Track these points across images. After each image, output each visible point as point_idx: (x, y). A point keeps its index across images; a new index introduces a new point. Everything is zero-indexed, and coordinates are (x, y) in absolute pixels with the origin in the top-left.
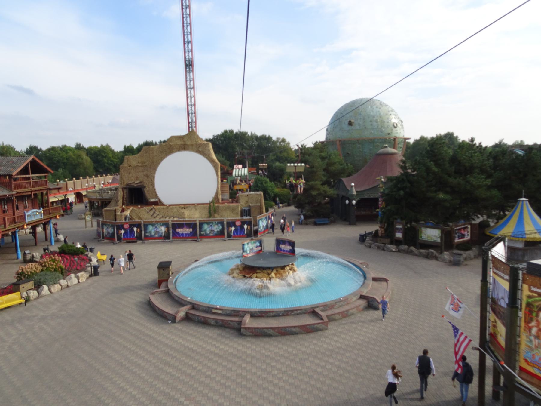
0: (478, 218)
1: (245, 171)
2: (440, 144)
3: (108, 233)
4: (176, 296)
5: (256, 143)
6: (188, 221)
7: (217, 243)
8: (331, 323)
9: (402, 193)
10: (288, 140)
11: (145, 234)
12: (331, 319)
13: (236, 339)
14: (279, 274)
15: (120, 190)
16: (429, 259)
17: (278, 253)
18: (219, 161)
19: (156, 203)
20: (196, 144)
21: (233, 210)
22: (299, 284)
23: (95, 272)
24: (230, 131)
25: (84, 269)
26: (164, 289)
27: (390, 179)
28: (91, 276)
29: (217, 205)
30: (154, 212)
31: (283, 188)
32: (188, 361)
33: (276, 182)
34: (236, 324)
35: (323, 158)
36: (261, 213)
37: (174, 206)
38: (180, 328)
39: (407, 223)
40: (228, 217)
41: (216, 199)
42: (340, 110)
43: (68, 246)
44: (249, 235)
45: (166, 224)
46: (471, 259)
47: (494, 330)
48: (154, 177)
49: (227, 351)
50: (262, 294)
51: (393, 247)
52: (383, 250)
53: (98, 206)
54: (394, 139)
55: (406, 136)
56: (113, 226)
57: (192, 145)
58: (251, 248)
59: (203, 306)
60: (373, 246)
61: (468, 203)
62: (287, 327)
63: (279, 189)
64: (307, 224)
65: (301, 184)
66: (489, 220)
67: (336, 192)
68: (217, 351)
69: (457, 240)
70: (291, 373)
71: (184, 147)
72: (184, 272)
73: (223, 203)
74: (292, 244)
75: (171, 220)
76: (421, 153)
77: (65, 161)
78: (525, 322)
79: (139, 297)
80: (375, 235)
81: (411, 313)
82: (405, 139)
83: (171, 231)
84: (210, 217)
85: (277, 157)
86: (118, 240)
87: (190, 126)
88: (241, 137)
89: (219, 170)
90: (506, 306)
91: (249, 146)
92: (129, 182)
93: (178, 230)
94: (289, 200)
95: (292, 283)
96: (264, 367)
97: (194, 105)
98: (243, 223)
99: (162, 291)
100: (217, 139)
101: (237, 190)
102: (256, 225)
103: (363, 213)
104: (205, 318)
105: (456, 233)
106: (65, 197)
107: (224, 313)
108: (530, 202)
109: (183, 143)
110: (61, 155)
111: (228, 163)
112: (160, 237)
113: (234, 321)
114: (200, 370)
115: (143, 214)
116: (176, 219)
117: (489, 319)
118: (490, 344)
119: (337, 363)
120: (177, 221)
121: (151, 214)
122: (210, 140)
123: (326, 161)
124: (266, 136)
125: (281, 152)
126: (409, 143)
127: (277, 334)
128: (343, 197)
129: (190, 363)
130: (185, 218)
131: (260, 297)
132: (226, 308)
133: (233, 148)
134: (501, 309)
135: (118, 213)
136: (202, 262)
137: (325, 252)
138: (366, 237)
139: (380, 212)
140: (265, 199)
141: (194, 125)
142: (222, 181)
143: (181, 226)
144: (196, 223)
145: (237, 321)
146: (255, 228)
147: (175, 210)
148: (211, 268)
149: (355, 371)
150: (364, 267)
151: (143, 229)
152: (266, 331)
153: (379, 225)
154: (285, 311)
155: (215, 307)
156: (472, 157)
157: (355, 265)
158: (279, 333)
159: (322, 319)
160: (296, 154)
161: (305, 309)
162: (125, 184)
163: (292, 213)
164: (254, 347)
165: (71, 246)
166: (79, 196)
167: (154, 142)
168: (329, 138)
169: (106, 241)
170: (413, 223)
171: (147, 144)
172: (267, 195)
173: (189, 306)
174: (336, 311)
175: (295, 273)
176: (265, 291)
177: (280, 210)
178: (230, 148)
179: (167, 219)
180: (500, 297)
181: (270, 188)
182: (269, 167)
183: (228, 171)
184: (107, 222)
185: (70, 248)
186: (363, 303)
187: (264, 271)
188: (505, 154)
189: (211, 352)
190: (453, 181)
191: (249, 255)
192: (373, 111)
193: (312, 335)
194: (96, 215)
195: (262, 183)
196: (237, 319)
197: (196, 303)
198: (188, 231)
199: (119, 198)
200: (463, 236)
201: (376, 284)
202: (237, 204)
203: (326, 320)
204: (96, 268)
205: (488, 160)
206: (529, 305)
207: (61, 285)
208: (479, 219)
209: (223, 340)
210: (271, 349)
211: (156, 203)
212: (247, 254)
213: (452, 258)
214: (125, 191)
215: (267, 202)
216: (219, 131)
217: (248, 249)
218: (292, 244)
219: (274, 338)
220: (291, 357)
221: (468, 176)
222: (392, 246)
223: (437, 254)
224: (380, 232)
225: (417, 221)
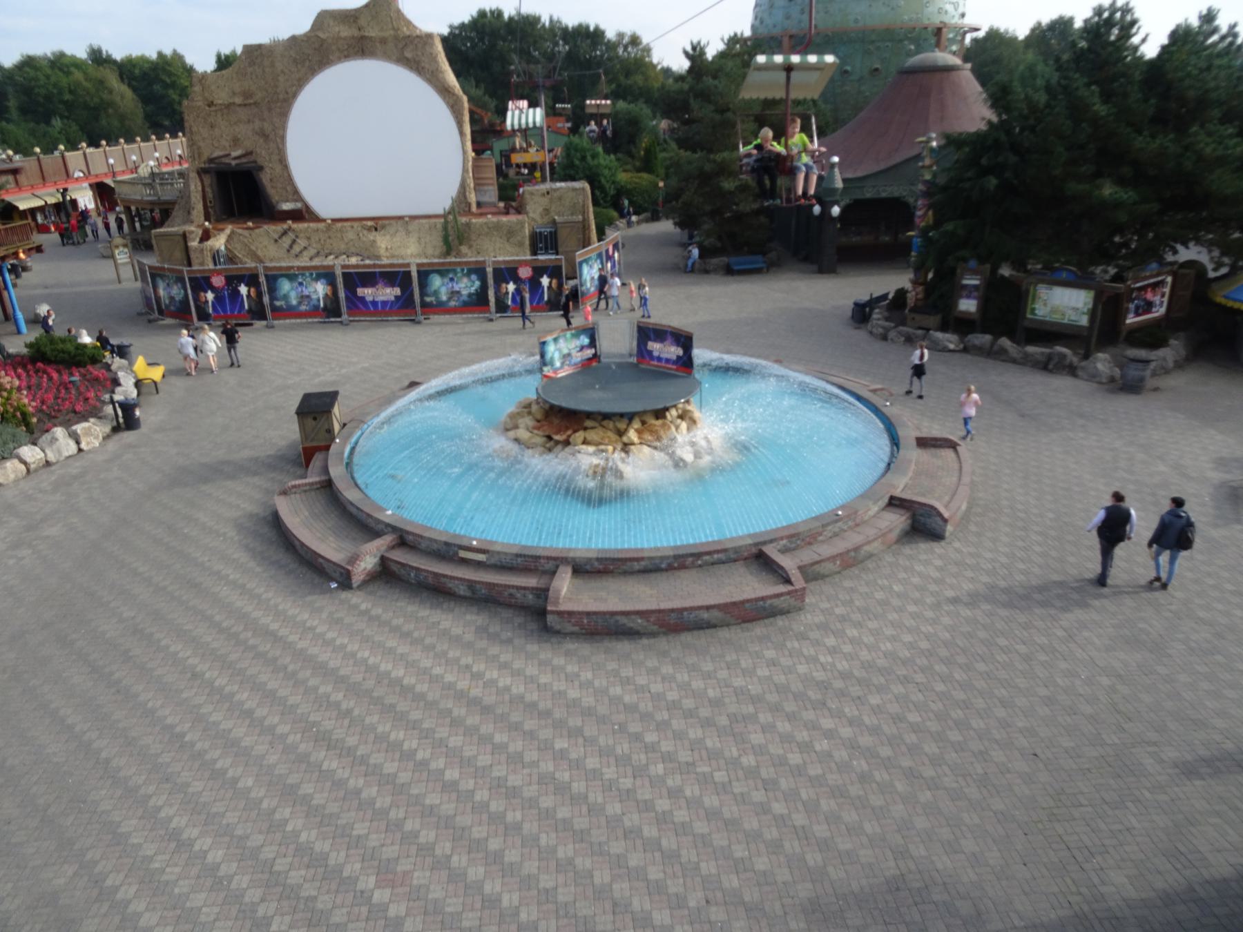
1: (536, 116)
3: (172, 298)
4: (351, 504)
5: (563, 48)
6: (384, 266)
7: (470, 327)
9: (993, 182)
10: (645, 40)
11: (272, 304)
12: (811, 573)
13: (532, 647)
14: (652, 432)
15: (193, 175)
16: (1051, 371)
17: (643, 366)
18: (465, 92)
20: (396, 38)
21: (510, 233)
22: (706, 460)
23: (127, 419)
24: (492, 12)
25: (94, 412)
26: (317, 479)
27: (953, 142)
28: (116, 429)
29: (464, 220)
30: (294, 242)
31: (639, 170)
32: (388, 727)
33: (620, 155)
34: (531, 597)
36: (586, 243)
37: (345, 224)
38: (363, 607)
40: (497, 253)
43: (52, 341)
45: (327, 276)
46: (1167, 372)
48: (283, 138)
49: (507, 689)
50: (603, 495)
51: (950, 340)
53: (142, 219)
56: (180, 280)
57: (383, 41)
58: (565, 351)
59: (431, 540)
60: (892, 334)
62: (685, 609)
63: (630, 175)
64: (706, 272)
68: (476, 692)
69: (1131, 320)
70: (706, 769)
71: (360, 48)
72: (377, 420)
73: (481, 215)
74: (685, 341)
75: (338, 263)
76: (1058, 60)
77: (67, 97)
79: (243, 498)
81: (1037, 549)
83: (342, 294)
84: (448, 253)
85: (619, 86)
86: (200, 319)
88: (524, 29)
89: (467, 118)
91: (544, 54)
92: (216, 154)
93: (361, 291)
94: (655, 203)
95: (689, 457)
96: (623, 748)
98: (539, 271)
99: (311, 484)
102: (572, 276)
103: (855, 239)
104: (436, 575)
105: (1132, 300)
106: (64, 195)
107: (493, 561)
109: (356, 33)
110: (53, 79)
111: (492, 104)
112: (315, 312)
113: (525, 588)
114: (424, 764)
115: (263, 245)
116: (354, 260)
119: (846, 732)
120: (357, 266)
121: (286, 245)
124: (588, 27)
125: (628, 74)
127: (655, 628)
129: (393, 736)
130: (378, 257)
131: (601, 501)
132: (497, 548)
133: (505, 62)
135: (194, 244)
138: (872, 310)
140: (596, 203)
143: (369, 279)
144: (409, 273)
145: (533, 589)
147: (351, 235)
149: (906, 762)
151: (265, 288)
152: (623, 620)
153: (911, 276)
154: (676, 557)
155: (465, 543)
156: (1209, 68)
158: (661, 626)
159: (788, 581)
161: (736, 550)
162: (205, 157)
163: (663, 241)
164: (589, 675)
165: (63, 341)
166: (103, 192)
168: (760, 31)
169: (169, 321)
172: (597, 193)
173: (388, 539)
174: (826, 550)
179: (330, 261)
183: (492, 125)
184: (163, 269)
185: (61, 346)
186: (897, 521)
187: (605, 423)
189: (460, 695)
190: (1146, 144)
191: (561, 374)
193: (758, 629)
194: (141, 244)
195: (583, 158)
196: (532, 582)
197: (408, 528)
198: (388, 293)
199: (193, 199)
200: (1149, 306)
201: (924, 456)
202: (520, 217)
203: (795, 575)
204: (128, 408)
207: (25, 463)
209: (494, 650)
210: (641, 680)
212: (555, 371)
214: (207, 180)
215: (598, 210)
216: (464, 14)
217: (557, 356)
218: (685, 341)
219: (645, 641)
220: (705, 712)
222: (948, 336)
223: (1075, 360)
224: (911, 299)
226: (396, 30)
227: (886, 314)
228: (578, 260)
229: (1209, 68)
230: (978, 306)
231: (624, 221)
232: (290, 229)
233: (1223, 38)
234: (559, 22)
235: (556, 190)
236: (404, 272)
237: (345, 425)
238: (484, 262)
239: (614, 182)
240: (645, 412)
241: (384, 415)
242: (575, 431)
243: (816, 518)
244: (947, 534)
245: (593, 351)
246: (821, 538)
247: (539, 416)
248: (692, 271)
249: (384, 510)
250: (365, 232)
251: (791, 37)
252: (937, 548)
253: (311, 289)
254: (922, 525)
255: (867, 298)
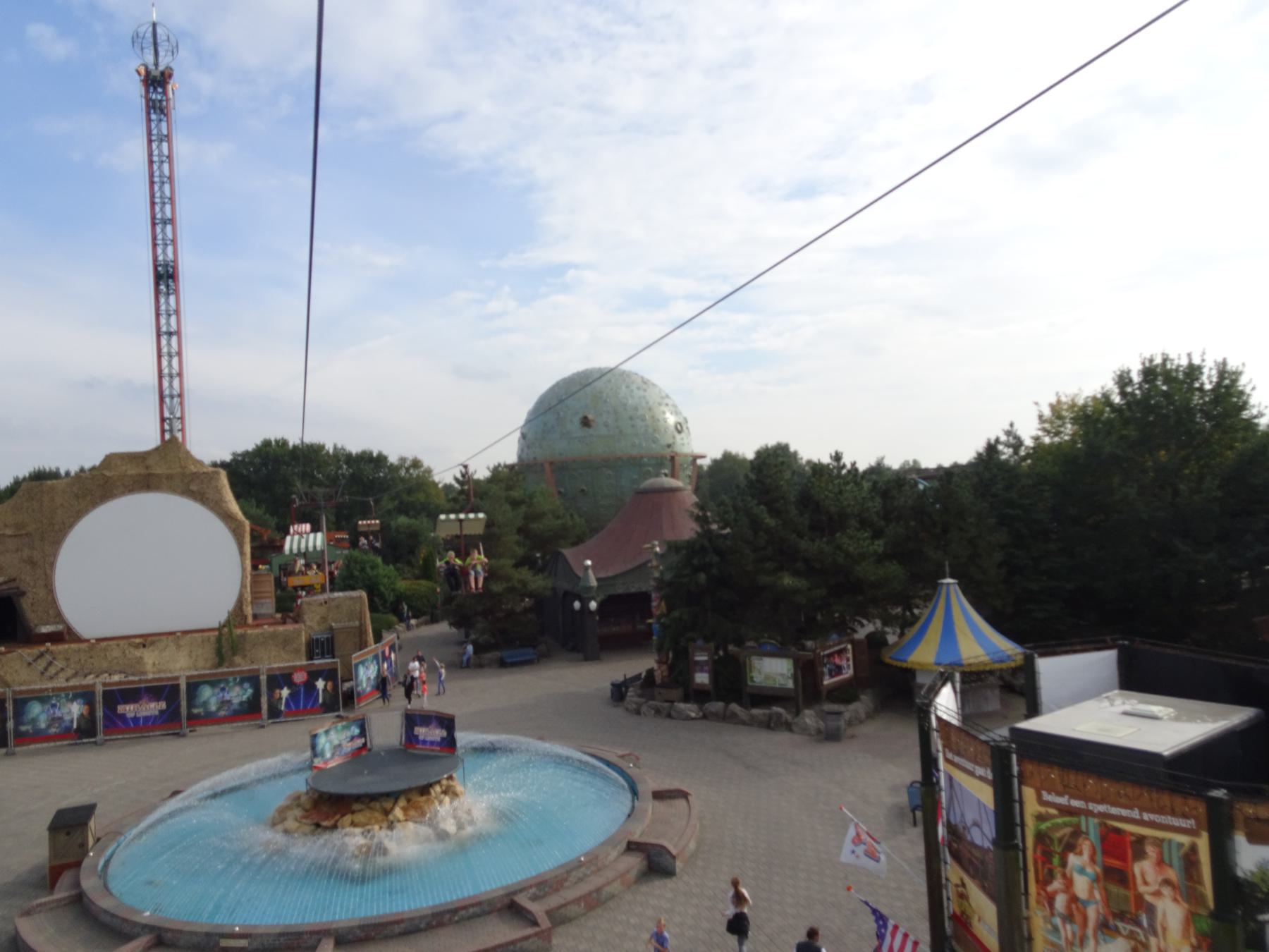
0: (863, 626)
2: (776, 466)
4: (105, 911)
6: (150, 681)
8: (560, 929)
9: (702, 577)
10: (426, 463)
12: (559, 918)
19: (56, 638)
21: (286, 642)
22: (469, 830)
24: (277, 442)
27: (673, 547)
29: (239, 631)
30: (50, 664)
31: (418, 578)
33: (399, 565)
35: (515, 504)
36: (362, 645)
37: (111, 643)
39: (717, 649)
40: (270, 661)
41: (237, 615)
42: (557, 385)
44: (330, 706)
45: (86, 695)
46: (861, 722)
47: (961, 905)
48: (52, 565)
51: (691, 709)
52: (669, 716)
54: (673, 458)
55: (697, 450)
57: (170, 477)
58: (336, 742)
59: (191, 933)
60: (644, 709)
61: (846, 593)
63: (409, 582)
64: (481, 666)
65: (479, 568)
66: (888, 629)
67: (549, 583)
69: (827, 681)
71: (147, 482)
72: (135, 831)
73: (257, 626)
74: (447, 723)
75: (99, 683)
78: (1037, 881)
80: (648, 682)
82: (695, 458)
83: (100, 713)
84: (220, 664)
87: (167, 427)
88: (309, 456)
89: (247, 539)
90: (987, 844)
95: (450, 826)
97: (180, 375)
100: (243, 461)
101: (295, 588)
103: (615, 629)
108: (959, 584)
109: (143, 471)
111: (273, 521)
116: (116, 678)
117: (947, 879)
118: (954, 943)
122: (224, 465)
123: (523, 509)
124: (371, 453)
126: (701, 467)
128: (566, 593)
130: (144, 673)
132: (260, 931)
134: (974, 851)
136: (190, 795)
137: (526, 735)
138: (627, 688)
139: (656, 627)
140: (373, 608)
141: (177, 425)
142: (255, 567)
143: (132, 695)
144: (178, 685)
146: (347, 685)
147: (116, 653)
148: (223, 812)
150: (630, 767)
155: (226, 930)
156: (841, 492)
157: (609, 764)
159: (535, 923)
160: (447, 495)
161: (490, 902)
167: (62, 472)
170: (731, 648)
171: (40, 477)
172: (376, 599)
174: (570, 894)
175: (456, 803)
176: (380, 860)
177: (410, 634)
178: (275, 484)
179: (90, 680)
180: (969, 823)
181: (386, 580)
182: (384, 527)
183: (272, 541)
186: (635, 862)
187: (372, 804)
188: (902, 486)
191: (332, 764)
192: (632, 397)
195: (363, 570)
197: (167, 925)
198: (152, 708)
200: (838, 670)
201: (661, 806)
202: (297, 626)
203: (545, 923)
205: (872, 498)
206: (1041, 837)
208: (865, 630)
211: (56, 638)
212: (326, 762)
213: (822, 725)
215: (376, 615)
216: (248, 443)
217: (328, 747)
218: (447, 723)
221: (838, 535)
222: (689, 706)
223: (789, 717)
225: (740, 642)
226: (184, 468)
227: (639, 692)
228: (354, 662)
229: (841, 492)
230: (710, 678)
231: (403, 625)
232: (48, 651)
233: (849, 472)
234: (343, 449)
235: (333, 600)
236: (172, 686)
237: (98, 840)
238: (258, 670)
239: (393, 590)
240: (409, 790)
241: (143, 825)
242: (343, 815)
243: (562, 866)
244: (678, 870)
245: (363, 740)
246: (567, 884)
247: (308, 806)
248: (468, 666)
249: (141, 912)
250: (132, 649)
251: (551, 463)
252: (669, 883)
253: (65, 710)
254: (656, 863)
255: (621, 679)
